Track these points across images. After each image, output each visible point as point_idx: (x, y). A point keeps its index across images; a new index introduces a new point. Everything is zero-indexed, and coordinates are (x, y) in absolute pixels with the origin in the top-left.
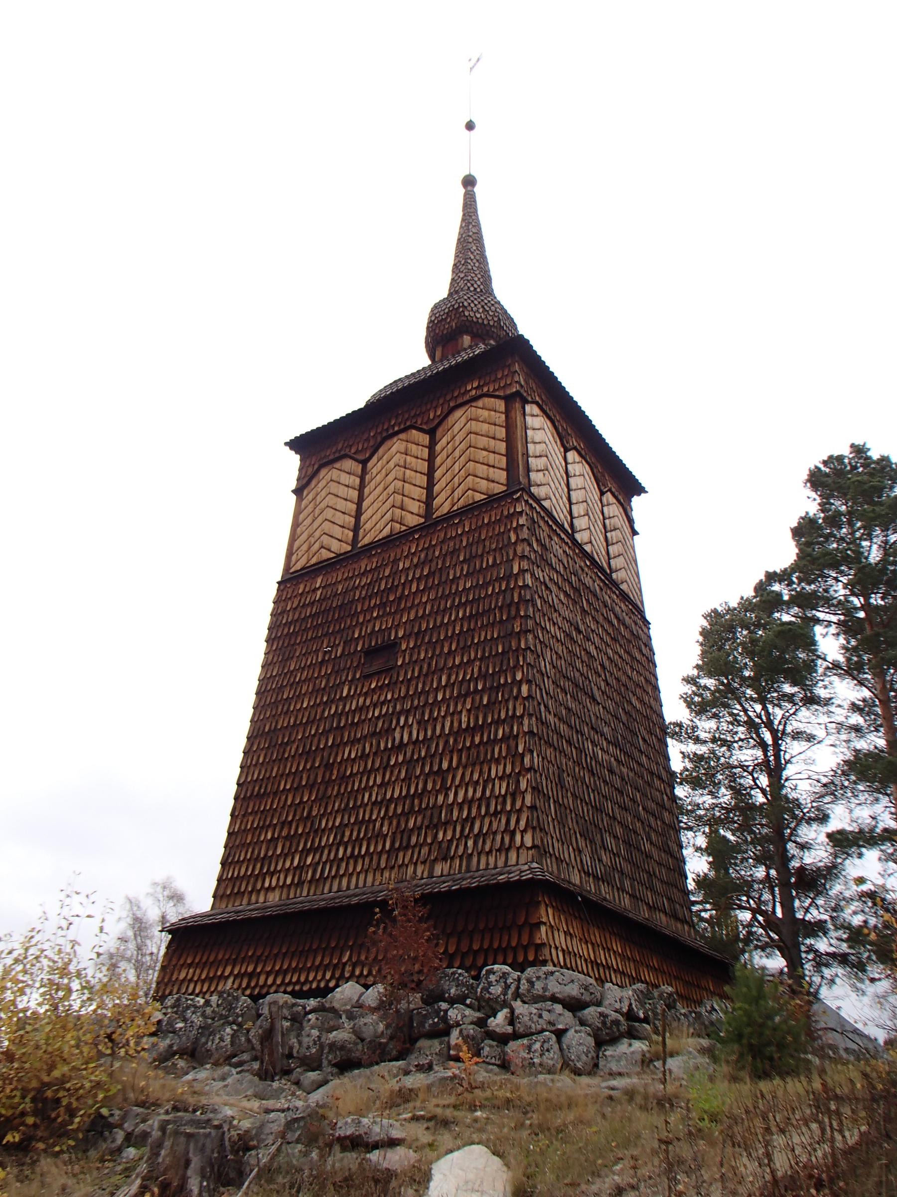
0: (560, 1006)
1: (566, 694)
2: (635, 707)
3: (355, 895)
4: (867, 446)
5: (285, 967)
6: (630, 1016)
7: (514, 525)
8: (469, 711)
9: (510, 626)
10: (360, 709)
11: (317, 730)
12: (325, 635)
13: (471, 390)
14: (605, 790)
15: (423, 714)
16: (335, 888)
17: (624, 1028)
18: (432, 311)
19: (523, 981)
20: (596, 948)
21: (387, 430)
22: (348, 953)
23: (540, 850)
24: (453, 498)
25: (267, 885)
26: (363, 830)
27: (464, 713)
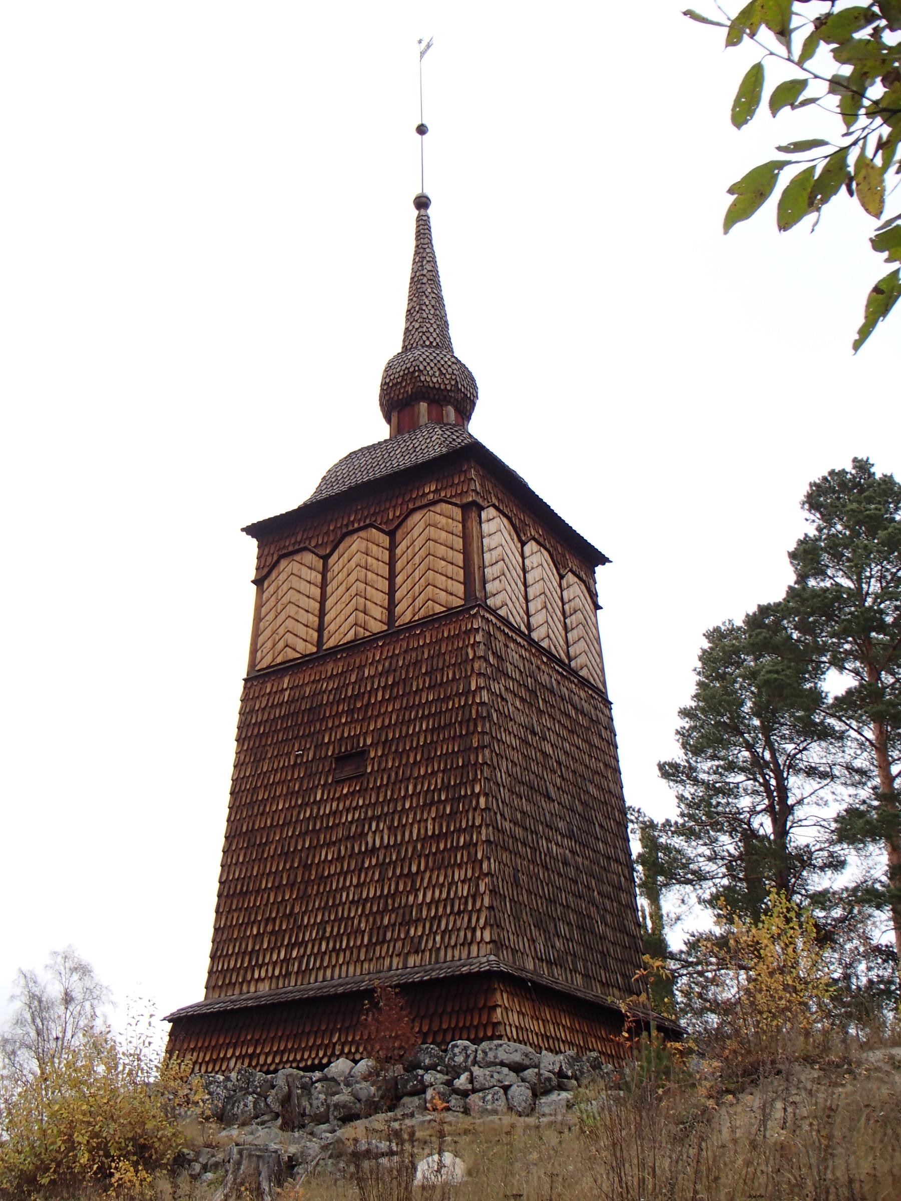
0: (507, 1069)
1: (521, 798)
2: (592, 796)
3: (340, 985)
4: (871, 461)
5: (282, 1048)
6: (561, 1074)
7: (472, 642)
8: (434, 819)
9: (469, 741)
10: (334, 813)
11: (294, 832)
12: (296, 738)
13: (428, 493)
14: (559, 882)
15: (393, 820)
16: (320, 978)
17: (555, 1082)
18: (386, 371)
19: (479, 1052)
20: (546, 1024)
21: (347, 525)
22: (337, 1035)
23: (498, 944)
24: (414, 606)
25: (256, 976)
26: (343, 927)
27: (430, 821)
